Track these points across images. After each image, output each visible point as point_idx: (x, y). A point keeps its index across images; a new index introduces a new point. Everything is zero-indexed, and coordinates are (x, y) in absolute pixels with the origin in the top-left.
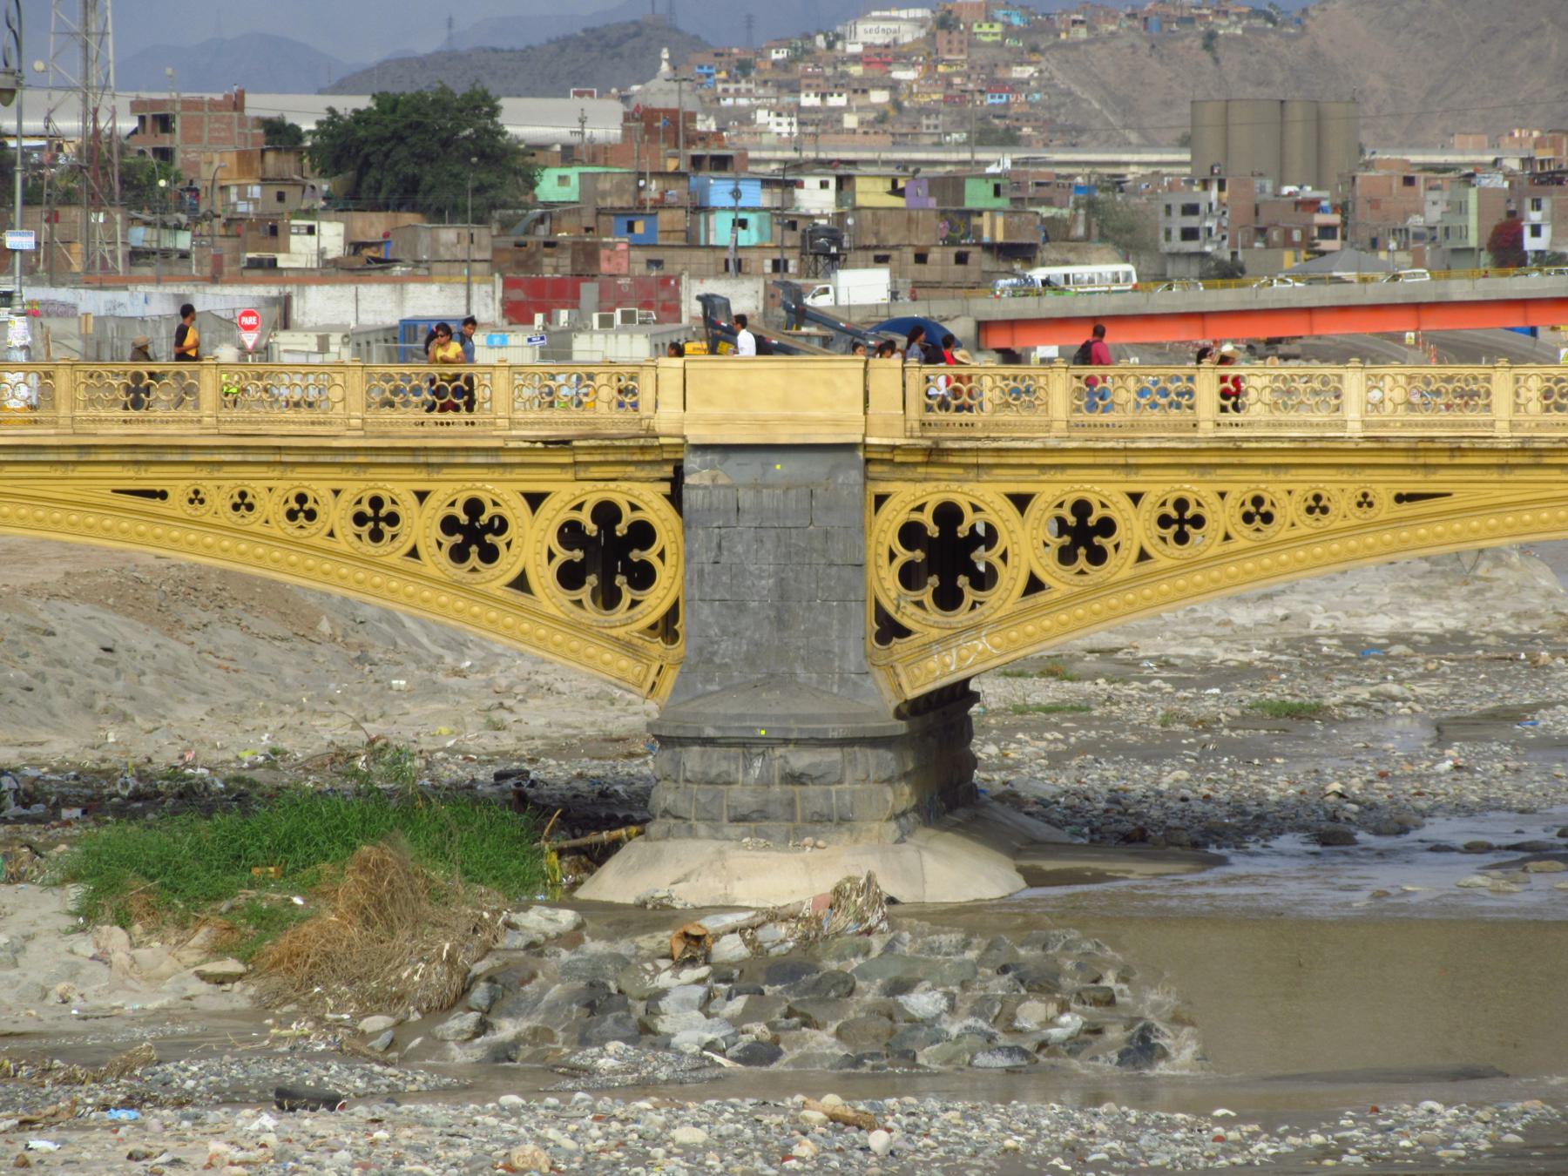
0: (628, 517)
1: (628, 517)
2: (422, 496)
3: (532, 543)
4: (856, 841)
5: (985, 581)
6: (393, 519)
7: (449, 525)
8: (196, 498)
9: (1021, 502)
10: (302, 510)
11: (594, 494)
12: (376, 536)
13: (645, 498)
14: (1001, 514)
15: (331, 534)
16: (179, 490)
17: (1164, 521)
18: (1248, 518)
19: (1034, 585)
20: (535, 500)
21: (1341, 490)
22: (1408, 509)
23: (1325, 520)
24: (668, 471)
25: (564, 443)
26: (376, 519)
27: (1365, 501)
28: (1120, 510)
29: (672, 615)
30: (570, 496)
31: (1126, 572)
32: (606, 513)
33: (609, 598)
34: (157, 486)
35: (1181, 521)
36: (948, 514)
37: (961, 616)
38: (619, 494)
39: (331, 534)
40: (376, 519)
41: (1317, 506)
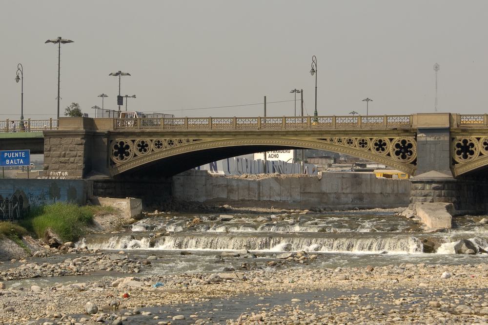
0: (125, 144)
1: (125, 144)
2: (371, 139)
3: (390, 147)
4: (233, 193)
5: (128, 154)
6: (366, 143)
7: (376, 144)
8: (332, 140)
9: (479, 139)
10: (350, 142)
11: (402, 138)
12: (363, 146)
13: (410, 139)
14: (130, 143)
15: (355, 146)
16: (328, 138)
17: (156, 145)
18: (169, 144)
19: (481, 154)
20: (391, 140)
21: (183, 139)
22: (195, 142)
23: (173, 146)
24: (415, 134)
25: (396, 129)
26: (363, 144)
27: (188, 141)
28: (149, 143)
29: (416, 160)
30: (397, 139)
31: (366, 151)
32: (404, 142)
33: (404, 157)
34: (325, 138)
35: (159, 145)
36: (465, 141)
37: (468, 160)
38: (406, 139)
39: (355, 146)
40: (363, 144)
41: (180, 142)
